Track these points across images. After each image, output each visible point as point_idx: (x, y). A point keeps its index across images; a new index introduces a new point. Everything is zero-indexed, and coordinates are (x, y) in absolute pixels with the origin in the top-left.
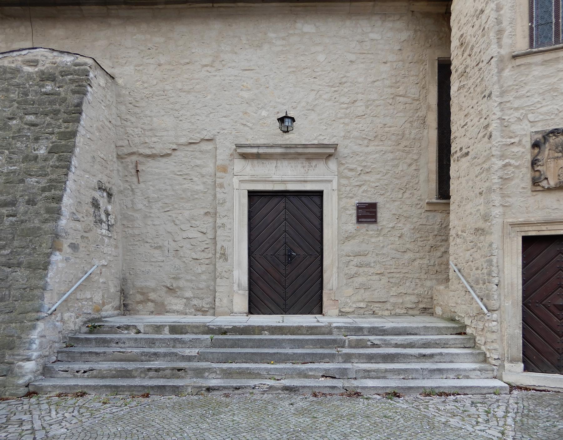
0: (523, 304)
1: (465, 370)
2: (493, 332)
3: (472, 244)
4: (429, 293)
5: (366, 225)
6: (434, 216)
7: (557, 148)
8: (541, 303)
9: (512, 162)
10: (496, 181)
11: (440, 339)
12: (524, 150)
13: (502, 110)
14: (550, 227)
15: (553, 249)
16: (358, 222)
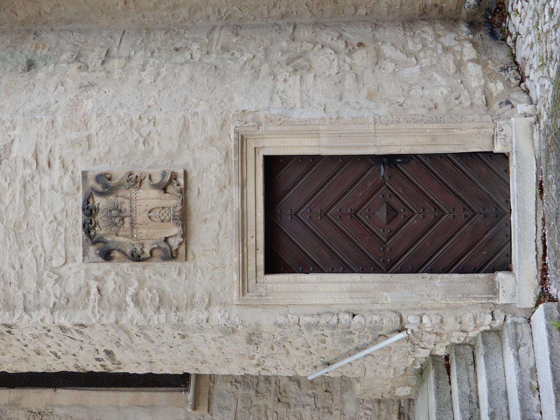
0: (387, 272)
1: (520, 376)
2: (442, 322)
3: (276, 348)
4: (370, 406)
6: (221, 395)
7: (116, 225)
8: (385, 244)
9: (131, 290)
10: (162, 317)
11: (462, 411)
12: (113, 273)
13: (38, 307)
14: (251, 233)
15: (288, 225)
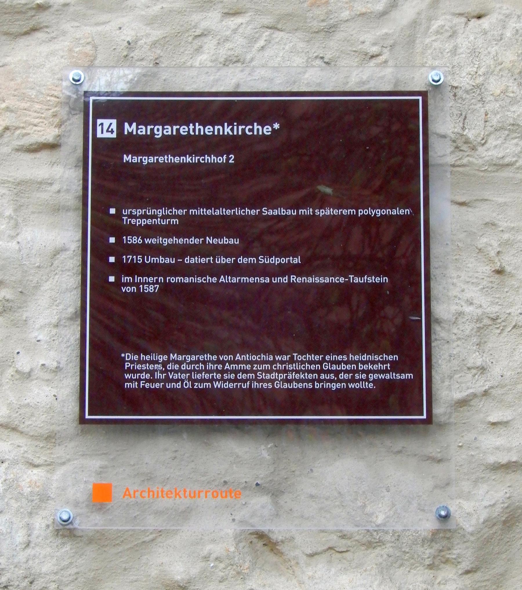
5: (239, 456)
6: (109, 84)
16: (110, 397)
